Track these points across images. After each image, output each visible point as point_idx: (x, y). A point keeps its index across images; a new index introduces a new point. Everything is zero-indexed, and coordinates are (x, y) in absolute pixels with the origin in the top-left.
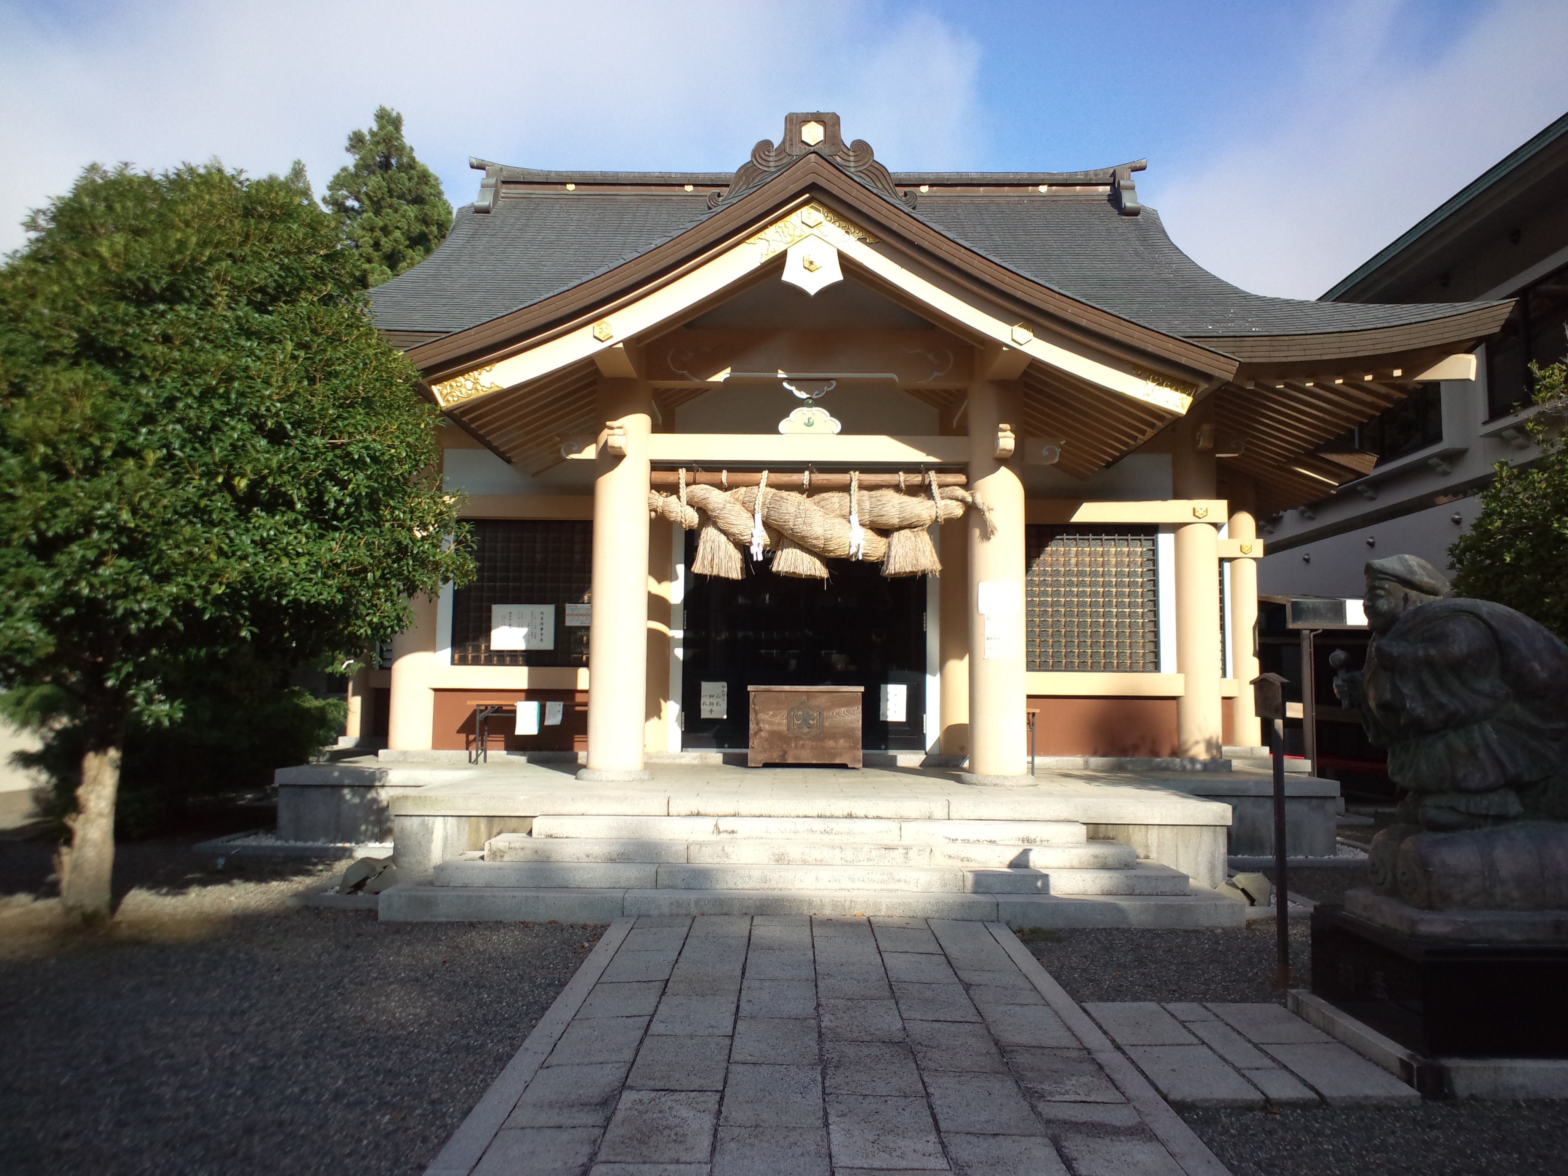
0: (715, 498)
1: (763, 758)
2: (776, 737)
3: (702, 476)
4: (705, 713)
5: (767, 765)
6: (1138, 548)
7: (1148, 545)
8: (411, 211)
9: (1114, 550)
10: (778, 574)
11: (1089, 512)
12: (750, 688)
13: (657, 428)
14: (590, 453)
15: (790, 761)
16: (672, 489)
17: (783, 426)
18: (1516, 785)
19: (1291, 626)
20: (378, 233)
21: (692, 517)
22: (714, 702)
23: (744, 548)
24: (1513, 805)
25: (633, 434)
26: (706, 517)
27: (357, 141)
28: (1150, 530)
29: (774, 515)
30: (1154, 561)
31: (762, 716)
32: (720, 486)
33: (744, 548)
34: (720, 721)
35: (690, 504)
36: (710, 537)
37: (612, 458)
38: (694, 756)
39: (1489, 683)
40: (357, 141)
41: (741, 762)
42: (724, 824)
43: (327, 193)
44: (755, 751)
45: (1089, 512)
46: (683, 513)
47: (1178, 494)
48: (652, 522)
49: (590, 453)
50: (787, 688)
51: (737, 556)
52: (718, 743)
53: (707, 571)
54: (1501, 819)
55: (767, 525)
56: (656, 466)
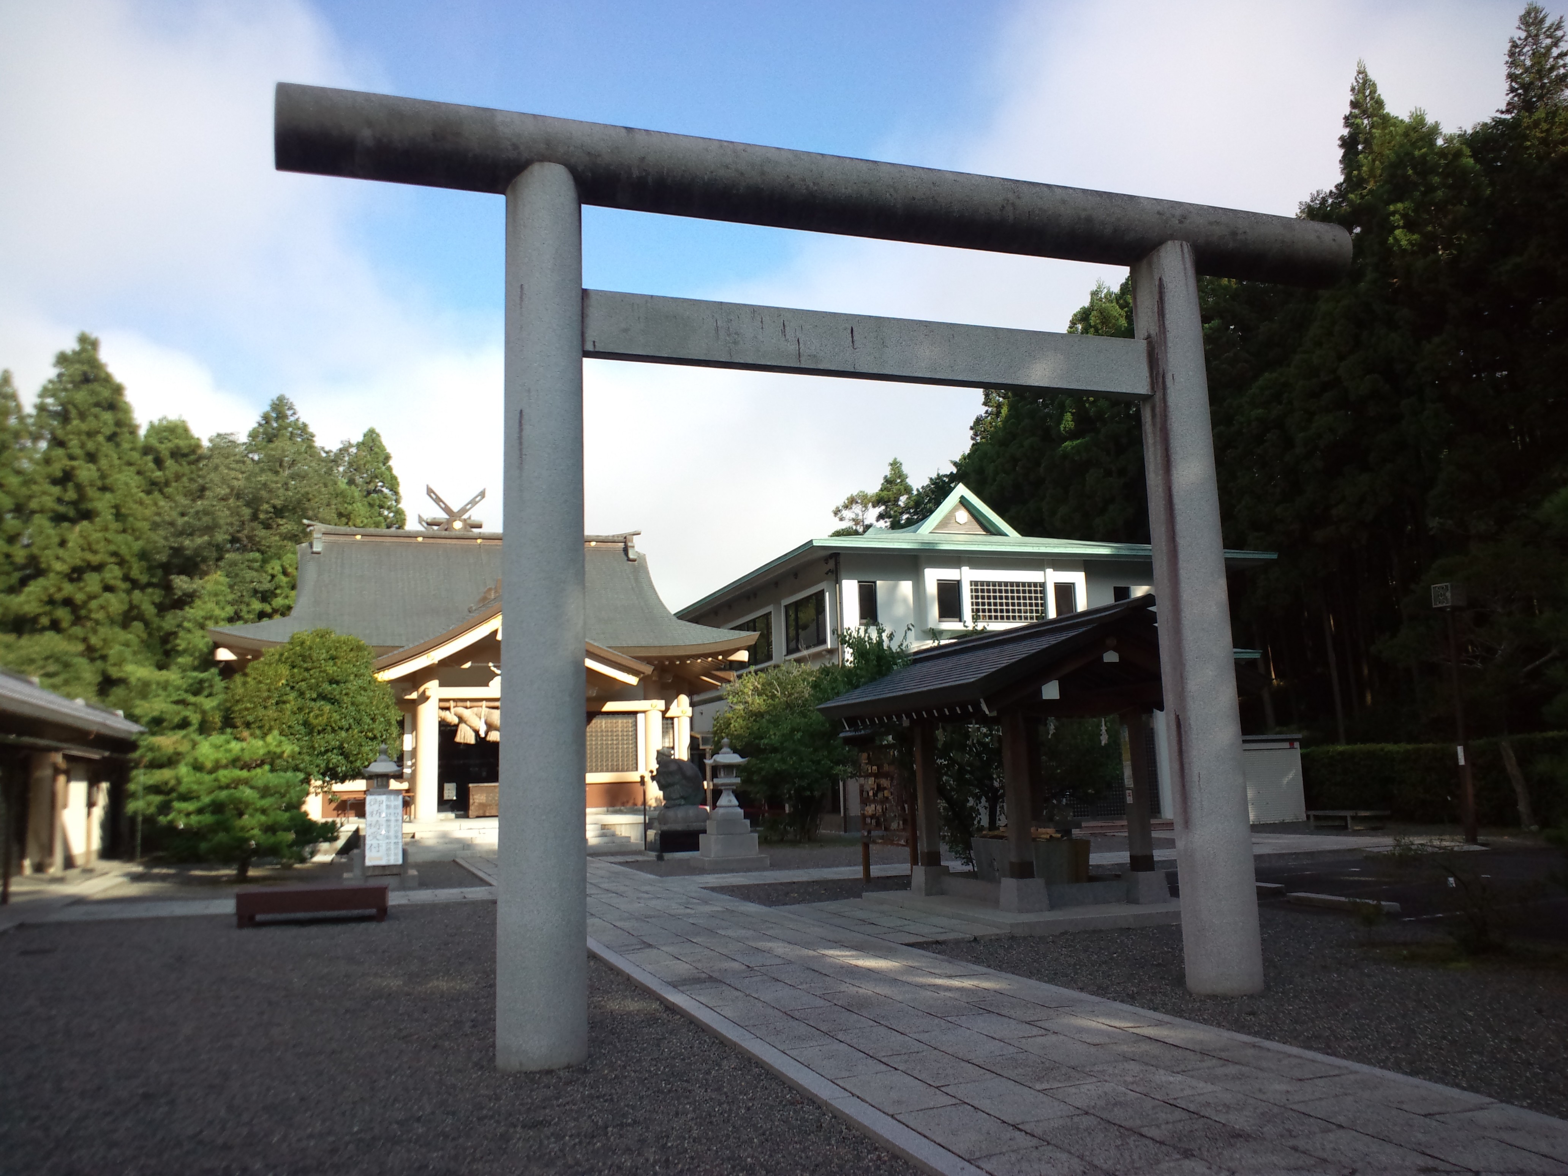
0: (467, 713)
1: (476, 814)
2: (482, 806)
3: (460, 704)
4: (446, 797)
5: (478, 817)
6: (630, 720)
7: (634, 719)
8: (108, 416)
9: (621, 722)
10: (489, 742)
11: (610, 706)
12: (471, 785)
13: (441, 685)
14: (414, 696)
15: (487, 814)
16: (448, 709)
17: (491, 683)
18: (682, 797)
19: (701, 747)
20: (84, 437)
21: (456, 720)
22: (451, 792)
23: (477, 733)
24: (683, 802)
25: (433, 688)
26: (461, 719)
27: (62, 359)
28: (634, 713)
29: (489, 720)
30: (636, 725)
31: (475, 797)
32: (466, 708)
33: (477, 733)
34: (452, 800)
35: (456, 715)
36: (463, 728)
37: (424, 698)
38: (443, 815)
39: (677, 778)
40: (62, 359)
41: (466, 816)
42: (482, 831)
43: (37, 401)
44: (472, 811)
45: (610, 706)
46: (451, 718)
47: (646, 698)
48: (440, 722)
49: (414, 696)
50: (486, 784)
51: (473, 734)
52: (452, 809)
53: (462, 741)
54: (680, 805)
55: (486, 723)
56: (441, 700)
